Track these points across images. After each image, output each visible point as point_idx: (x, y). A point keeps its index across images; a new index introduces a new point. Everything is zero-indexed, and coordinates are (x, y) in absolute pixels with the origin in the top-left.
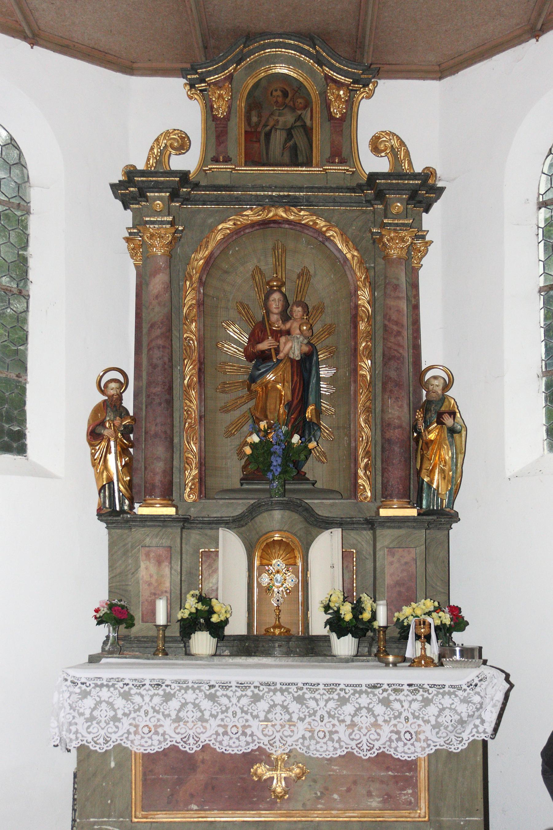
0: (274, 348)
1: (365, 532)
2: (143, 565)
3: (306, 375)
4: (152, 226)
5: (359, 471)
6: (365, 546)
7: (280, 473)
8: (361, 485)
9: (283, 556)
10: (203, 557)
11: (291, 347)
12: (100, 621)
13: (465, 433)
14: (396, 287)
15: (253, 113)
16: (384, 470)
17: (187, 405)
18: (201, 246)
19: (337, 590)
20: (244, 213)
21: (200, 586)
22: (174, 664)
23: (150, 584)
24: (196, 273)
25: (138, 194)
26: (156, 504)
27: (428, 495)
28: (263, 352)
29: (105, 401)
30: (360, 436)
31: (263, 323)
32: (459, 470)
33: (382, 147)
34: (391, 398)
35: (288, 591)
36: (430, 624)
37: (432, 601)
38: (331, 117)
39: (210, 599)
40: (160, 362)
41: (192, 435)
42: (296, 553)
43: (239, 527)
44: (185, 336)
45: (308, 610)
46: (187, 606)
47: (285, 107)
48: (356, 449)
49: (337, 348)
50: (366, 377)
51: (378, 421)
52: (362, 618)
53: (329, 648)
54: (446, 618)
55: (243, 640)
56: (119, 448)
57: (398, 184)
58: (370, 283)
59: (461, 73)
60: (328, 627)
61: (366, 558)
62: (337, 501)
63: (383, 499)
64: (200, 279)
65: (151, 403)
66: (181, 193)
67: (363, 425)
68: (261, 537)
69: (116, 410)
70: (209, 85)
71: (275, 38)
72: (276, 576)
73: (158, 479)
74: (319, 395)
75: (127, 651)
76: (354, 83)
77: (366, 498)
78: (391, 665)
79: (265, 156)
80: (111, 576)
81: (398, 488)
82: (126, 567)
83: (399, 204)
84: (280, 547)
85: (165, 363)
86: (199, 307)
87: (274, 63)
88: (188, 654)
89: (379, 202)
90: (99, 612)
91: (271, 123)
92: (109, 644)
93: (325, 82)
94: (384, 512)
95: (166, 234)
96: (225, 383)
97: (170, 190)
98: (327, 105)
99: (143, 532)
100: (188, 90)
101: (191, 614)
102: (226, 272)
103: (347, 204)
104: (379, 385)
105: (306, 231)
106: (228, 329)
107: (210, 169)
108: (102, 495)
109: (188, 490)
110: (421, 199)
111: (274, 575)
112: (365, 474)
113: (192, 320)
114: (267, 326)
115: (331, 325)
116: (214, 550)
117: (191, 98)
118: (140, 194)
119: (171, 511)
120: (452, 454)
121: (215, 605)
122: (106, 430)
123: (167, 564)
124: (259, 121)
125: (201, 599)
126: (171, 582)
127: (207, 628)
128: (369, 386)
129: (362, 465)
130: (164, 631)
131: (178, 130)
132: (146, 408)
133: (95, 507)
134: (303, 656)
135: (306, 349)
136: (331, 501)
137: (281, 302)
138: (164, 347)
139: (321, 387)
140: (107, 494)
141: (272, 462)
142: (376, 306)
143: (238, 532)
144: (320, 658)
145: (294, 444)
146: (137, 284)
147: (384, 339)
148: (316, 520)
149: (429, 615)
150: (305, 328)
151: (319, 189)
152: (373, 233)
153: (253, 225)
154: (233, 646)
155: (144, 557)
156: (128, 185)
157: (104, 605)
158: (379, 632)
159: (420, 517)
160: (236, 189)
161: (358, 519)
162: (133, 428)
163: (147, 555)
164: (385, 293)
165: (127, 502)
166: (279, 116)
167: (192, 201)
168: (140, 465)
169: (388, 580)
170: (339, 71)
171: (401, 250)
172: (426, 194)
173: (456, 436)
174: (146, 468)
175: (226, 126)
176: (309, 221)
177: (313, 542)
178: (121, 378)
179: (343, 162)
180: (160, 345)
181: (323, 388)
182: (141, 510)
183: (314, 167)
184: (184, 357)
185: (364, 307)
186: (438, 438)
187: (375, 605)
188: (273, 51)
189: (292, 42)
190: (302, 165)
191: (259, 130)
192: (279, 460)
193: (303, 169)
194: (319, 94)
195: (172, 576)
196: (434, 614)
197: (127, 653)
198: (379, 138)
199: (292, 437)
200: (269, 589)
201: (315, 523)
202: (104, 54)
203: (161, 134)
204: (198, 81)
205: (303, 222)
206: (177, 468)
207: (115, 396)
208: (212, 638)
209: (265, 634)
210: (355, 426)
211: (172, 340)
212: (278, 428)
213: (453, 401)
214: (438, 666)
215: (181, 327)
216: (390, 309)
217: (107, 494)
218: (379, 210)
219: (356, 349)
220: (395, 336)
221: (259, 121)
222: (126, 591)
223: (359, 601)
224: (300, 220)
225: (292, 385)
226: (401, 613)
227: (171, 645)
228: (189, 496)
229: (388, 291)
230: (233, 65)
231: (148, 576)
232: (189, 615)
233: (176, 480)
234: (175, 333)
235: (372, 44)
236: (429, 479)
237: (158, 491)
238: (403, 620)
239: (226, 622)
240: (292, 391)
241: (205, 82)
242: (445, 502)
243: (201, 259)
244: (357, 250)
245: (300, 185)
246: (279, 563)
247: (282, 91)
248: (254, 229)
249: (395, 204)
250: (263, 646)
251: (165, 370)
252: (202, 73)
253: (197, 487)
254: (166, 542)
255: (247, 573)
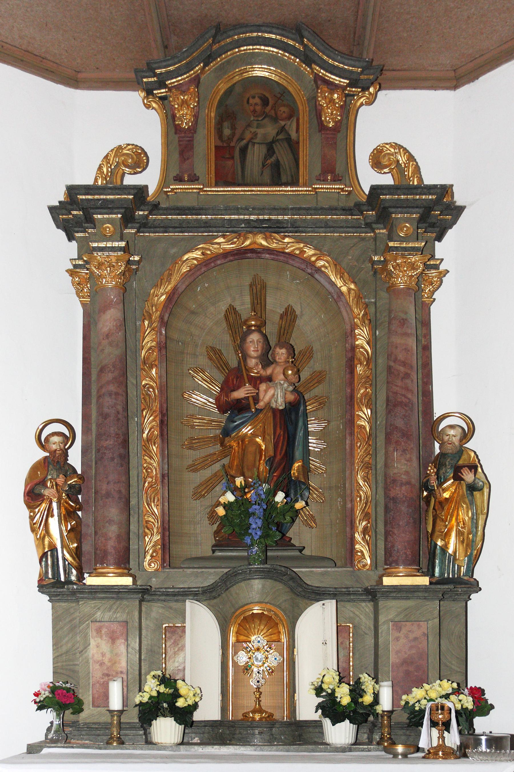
0: (252, 396)
1: (363, 604)
2: (93, 643)
3: (291, 428)
4: (99, 254)
5: (356, 535)
6: (364, 619)
7: (260, 537)
8: (358, 552)
9: (265, 631)
10: (167, 633)
11: (274, 395)
12: (41, 706)
13: (488, 490)
14: (403, 322)
15: (226, 124)
16: (387, 534)
17: (146, 462)
18: (162, 280)
19: (331, 669)
20: (215, 241)
21: (164, 666)
22: (130, 756)
23: (102, 664)
24: (157, 310)
25: (83, 218)
26: (109, 573)
27: (442, 562)
28: (239, 401)
29: (46, 458)
30: (357, 496)
31: (239, 369)
32: (480, 533)
33: (385, 162)
34: (397, 450)
35: (271, 671)
36: (450, 710)
37: (450, 682)
38: (322, 127)
39: (176, 681)
40: (112, 411)
41: (153, 495)
42: (281, 628)
43: (210, 599)
44: (143, 383)
45: (294, 692)
46: (146, 688)
47: (265, 118)
48: (353, 510)
49: (328, 398)
50: (364, 428)
51: (380, 478)
52: (363, 702)
53: (320, 735)
54: (468, 703)
55: (216, 726)
56: (63, 510)
57: (407, 200)
58: (370, 320)
59: (482, 79)
60: (320, 711)
61: (366, 634)
62: (329, 569)
63: (386, 567)
64: (161, 318)
65: (102, 458)
66: (137, 217)
67: (361, 482)
68: (237, 610)
69: (60, 468)
70: (170, 90)
71: (252, 32)
72: (256, 654)
73: (111, 545)
74: (307, 452)
75: (74, 739)
76: (350, 85)
77: (364, 566)
78: (400, 757)
79: (240, 172)
80: (56, 655)
81: (405, 553)
82: (73, 646)
83: (407, 225)
84: (261, 621)
85: (118, 413)
86: (160, 350)
87: (252, 64)
88: (149, 742)
89: (382, 226)
90: (40, 696)
91: (248, 136)
92: (52, 732)
93: (315, 85)
94: (387, 581)
95: (117, 263)
96: (192, 439)
97: (123, 211)
98: (318, 112)
99: (93, 606)
100: (145, 97)
101: (151, 697)
102: (193, 313)
103: (342, 229)
104: (381, 438)
105: (291, 262)
106: (196, 377)
107: (173, 189)
108: (43, 563)
109: (148, 557)
110: (433, 220)
111: (254, 653)
112: (364, 539)
113: (152, 365)
114: (244, 371)
115: (320, 372)
116: (180, 625)
117: (148, 106)
118: (86, 218)
119: (128, 581)
120: (472, 514)
121: (181, 687)
122: (47, 490)
123: (123, 641)
124: (233, 134)
125: (164, 680)
126: (127, 662)
127: (171, 714)
128: (368, 438)
129: (360, 528)
130: (119, 717)
131: (133, 145)
132: (96, 463)
133: (36, 578)
134: (290, 745)
135: (291, 397)
136: (322, 569)
137: (260, 344)
138: (117, 394)
139: (309, 443)
140: (49, 562)
141: (250, 524)
142: (378, 346)
143: (209, 604)
144: (311, 747)
145: (278, 503)
146: (83, 324)
147: (388, 383)
148: (304, 591)
149: (446, 699)
150: (290, 372)
151: (308, 211)
152: (373, 263)
153: (226, 254)
154: (203, 733)
155: (95, 634)
156: (70, 207)
157: (46, 687)
158: (382, 716)
159: (433, 587)
160: (204, 211)
161: (356, 589)
162: (81, 488)
163: (99, 631)
164: (389, 330)
165: (74, 572)
166: (257, 128)
167: (150, 227)
168: (88, 530)
169: (393, 658)
170: (333, 70)
171: (410, 279)
172: (440, 215)
173: (477, 494)
174: (96, 533)
175: (191, 141)
176: (295, 249)
177: (300, 615)
178: (65, 431)
179: (336, 179)
180: (112, 391)
181: (311, 443)
182: (90, 581)
183: (301, 187)
184: (143, 407)
185: (363, 347)
186: (456, 495)
187: (377, 686)
188: (250, 49)
189: (273, 36)
190: (286, 185)
191: (232, 144)
192: (260, 523)
193: (287, 189)
194: (307, 100)
195: (129, 655)
196: (453, 698)
197: (75, 741)
198: (381, 151)
199: (275, 495)
200: (247, 669)
201: (303, 594)
202: (41, 59)
203: (112, 150)
204: (157, 85)
205: (287, 251)
206: (135, 533)
207: (58, 452)
208: (178, 725)
209: (242, 720)
210: (351, 483)
211: (127, 387)
212: (258, 485)
213: (472, 454)
214: (459, 758)
215: (138, 373)
216: (396, 347)
217: (49, 562)
218: (381, 235)
219: (352, 397)
220: (403, 378)
221: (233, 134)
222: (74, 671)
223: (358, 682)
224: (284, 248)
225: (274, 439)
226: (410, 696)
227: (127, 732)
228: (149, 565)
229: (393, 327)
230: (199, 64)
231: (100, 655)
232: (149, 699)
233: (133, 546)
234: (131, 380)
235: (374, 39)
236: (443, 543)
237: (111, 558)
238: (414, 704)
239: (195, 706)
240: (274, 445)
241: (165, 86)
242: (463, 570)
243: (162, 295)
244: (354, 282)
245: (283, 206)
246: (259, 639)
247: (261, 98)
248: (227, 260)
249: (403, 225)
250: (240, 733)
251: (118, 420)
252: (161, 74)
253: (160, 555)
254: (121, 616)
255: (221, 651)
